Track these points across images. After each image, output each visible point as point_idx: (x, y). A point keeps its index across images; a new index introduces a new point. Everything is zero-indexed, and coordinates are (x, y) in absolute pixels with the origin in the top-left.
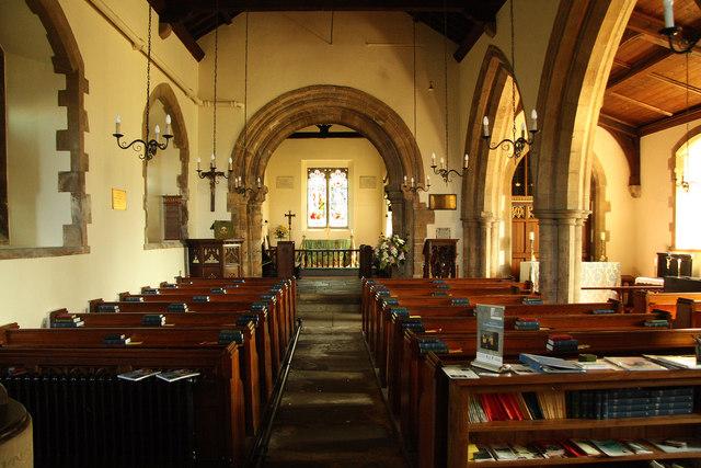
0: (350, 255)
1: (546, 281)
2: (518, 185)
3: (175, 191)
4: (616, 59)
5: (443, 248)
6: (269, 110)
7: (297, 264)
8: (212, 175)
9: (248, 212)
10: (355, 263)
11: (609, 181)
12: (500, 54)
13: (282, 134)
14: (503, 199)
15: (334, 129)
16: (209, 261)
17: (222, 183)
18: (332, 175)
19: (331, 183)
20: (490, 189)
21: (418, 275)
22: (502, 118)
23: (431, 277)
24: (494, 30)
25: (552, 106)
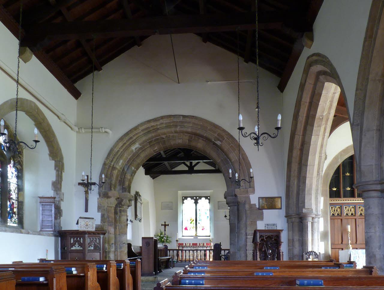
1: (374, 256)
2: (335, 189)
3: (51, 193)
5: (269, 237)
6: (131, 135)
8: (87, 185)
9: (116, 213)
10: (210, 257)
14: (322, 199)
16: (74, 248)
17: (95, 189)
18: (199, 201)
20: (311, 189)
21: (250, 258)
22: (319, 126)
23: (259, 259)
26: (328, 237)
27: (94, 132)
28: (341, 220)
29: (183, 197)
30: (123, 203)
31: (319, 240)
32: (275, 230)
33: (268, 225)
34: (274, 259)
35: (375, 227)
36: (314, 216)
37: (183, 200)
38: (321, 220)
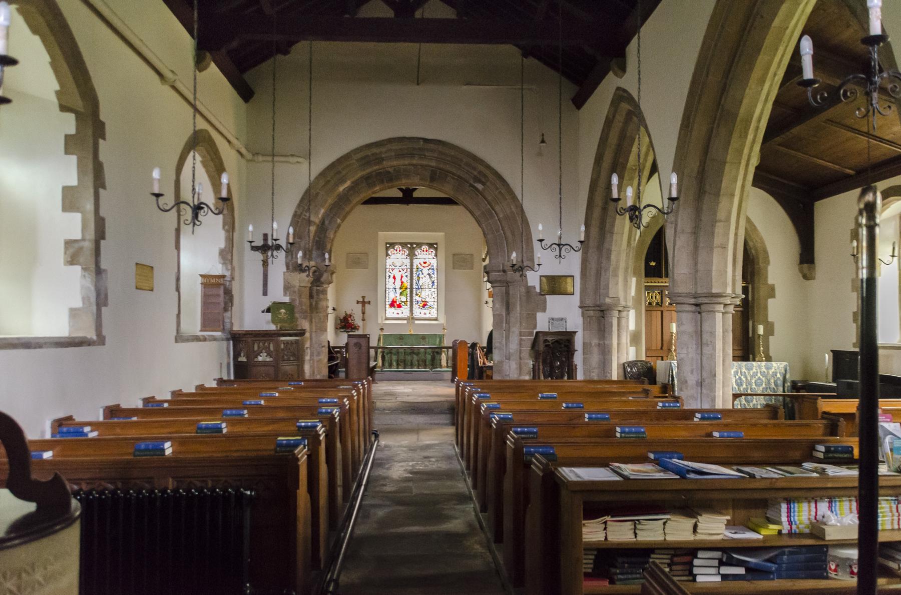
0: (439, 353)
2: (653, 264)
4: (776, 103)
7: (372, 364)
8: (266, 248)
11: (772, 258)
12: (629, 98)
13: (356, 199)
15: (421, 192)
16: (260, 359)
17: (280, 257)
18: (417, 252)
19: (416, 262)
24: (623, 69)
25: (693, 165)
26: (641, 345)
27: (276, 162)
28: (662, 312)
29: (387, 243)
30: (322, 280)
31: (629, 344)
32: (564, 332)
33: (553, 319)
34: (562, 377)
35: (688, 348)
36: (621, 309)
37: (387, 249)
38: (632, 314)
